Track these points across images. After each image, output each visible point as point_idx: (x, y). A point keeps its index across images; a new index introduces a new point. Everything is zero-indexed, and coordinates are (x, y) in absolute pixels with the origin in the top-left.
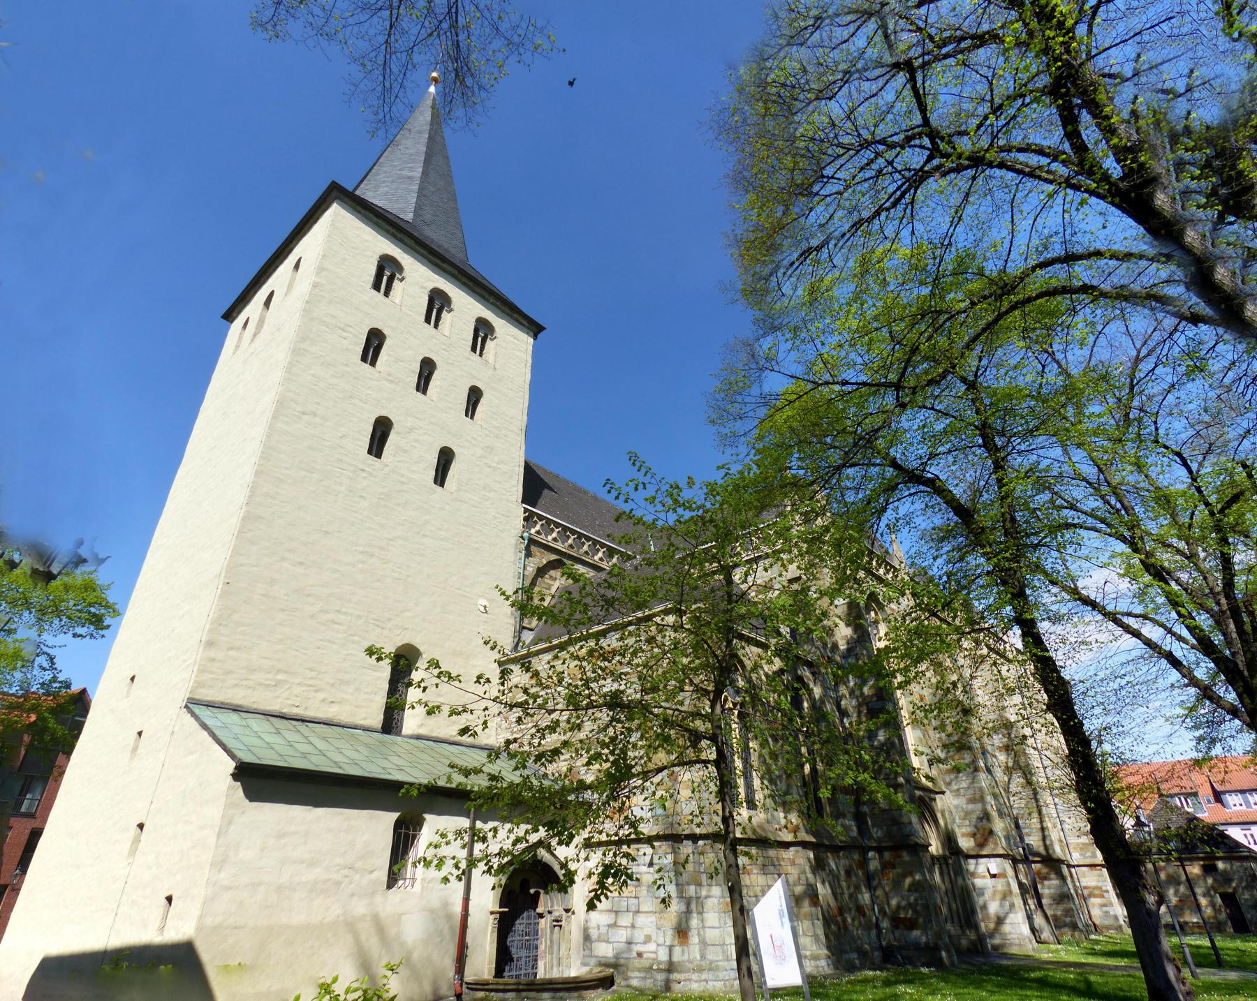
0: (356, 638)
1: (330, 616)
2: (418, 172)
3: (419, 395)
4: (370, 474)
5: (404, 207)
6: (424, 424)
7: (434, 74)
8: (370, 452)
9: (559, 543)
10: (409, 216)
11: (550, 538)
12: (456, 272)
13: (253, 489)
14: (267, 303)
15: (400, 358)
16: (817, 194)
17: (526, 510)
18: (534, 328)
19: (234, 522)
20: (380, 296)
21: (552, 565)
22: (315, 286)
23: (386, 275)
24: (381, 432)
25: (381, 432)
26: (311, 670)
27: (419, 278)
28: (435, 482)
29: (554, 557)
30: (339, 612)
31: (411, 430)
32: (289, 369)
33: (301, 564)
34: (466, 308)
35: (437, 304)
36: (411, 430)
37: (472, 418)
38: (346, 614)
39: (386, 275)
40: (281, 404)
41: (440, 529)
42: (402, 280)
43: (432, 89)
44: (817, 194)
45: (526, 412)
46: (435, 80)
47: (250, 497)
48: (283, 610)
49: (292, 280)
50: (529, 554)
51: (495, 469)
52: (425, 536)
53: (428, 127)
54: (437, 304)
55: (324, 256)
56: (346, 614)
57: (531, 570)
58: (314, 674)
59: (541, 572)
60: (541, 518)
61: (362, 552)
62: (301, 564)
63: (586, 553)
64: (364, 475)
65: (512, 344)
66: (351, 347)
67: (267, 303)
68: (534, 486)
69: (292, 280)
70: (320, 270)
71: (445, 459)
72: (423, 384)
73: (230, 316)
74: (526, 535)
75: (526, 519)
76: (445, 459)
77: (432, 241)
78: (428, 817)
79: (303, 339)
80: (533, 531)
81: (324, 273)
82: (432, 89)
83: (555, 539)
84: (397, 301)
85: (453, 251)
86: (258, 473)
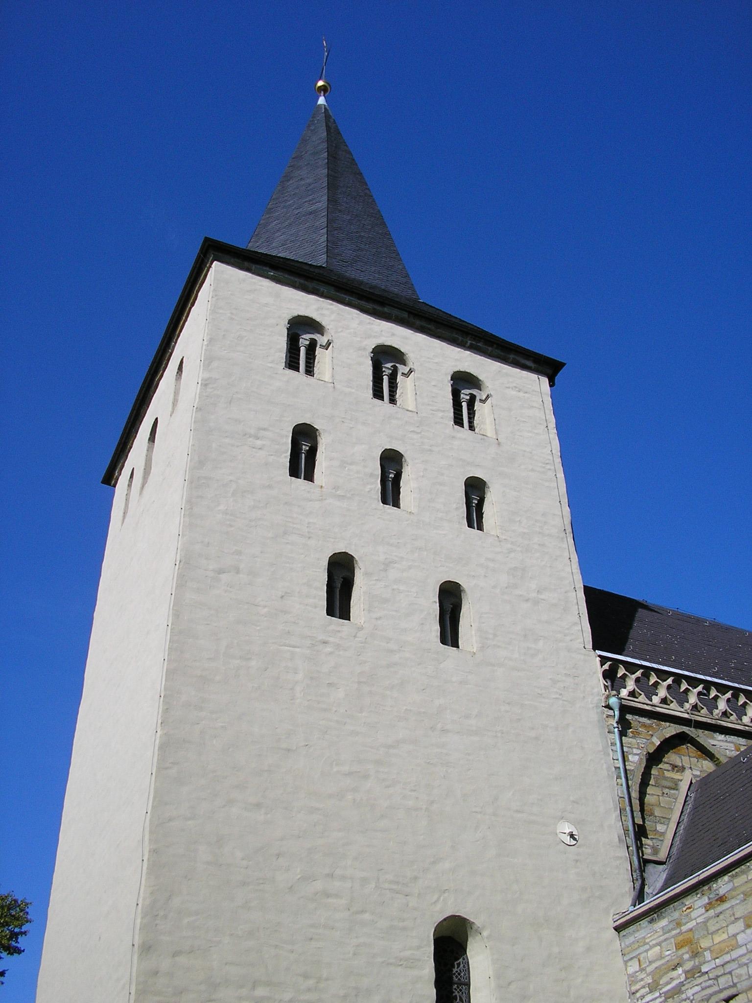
0: (367, 916)
1: (318, 885)
2: (322, 202)
3: (389, 509)
4: (338, 646)
5: (312, 250)
6: (407, 553)
7: (321, 83)
8: (330, 612)
9: (674, 705)
10: (321, 260)
11: (656, 700)
12: (405, 315)
13: (169, 698)
14: (152, 438)
15: (348, 461)
16: (648, 943)
17: (604, 660)
18: (548, 367)
19: (149, 756)
20: (299, 377)
21: (669, 744)
22: (205, 384)
23: (301, 345)
24: (341, 581)
25: (341, 581)
26: (306, 976)
27: (351, 332)
28: (443, 641)
29: (671, 730)
30: (331, 876)
31: (387, 565)
32: (191, 504)
33: (258, 806)
34: (432, 360)
35: (386, 364)
36: (387, 565)
37: (480, 528)
38: (343, 878)
39: (301, 345)
40: (187, 565)
41: (467, 717)
42: (327, 346)
43: (322, 101)
44: (648, 943)
45: (565, 501)
46: (324, 89)
47: (166, 711)
48: (244, 884)
49: (176, 393)
50: (624, 727)
51: (536, 602)
52: (444, 731)
53: (325, 145)
54: (386, 364)
55: (211, 340)
56: (343, 878)
57: (636, 760)
58: (311, 982)
59: (654, 758)
60: (631, 668)
61: (350, 774)
62: (258, 806)
63: (725, 714)
64: (329, 649)
65: (518, 400)
66: (271, 459)
67: (152, 438)
68: (611, 619)
69: (176, 393)
70: (208, 361)
71: (450, 598)
72: (391, 492)
73: (110, 478)
74: (613, 701)
75: (607, 675)
76: (450, 598)
77: (361, 283)
78: (235, 315)
79: (201, 463)
80: (624, 693)
81: (215, 364)
82: (322, 101)
83: (664, 701)
84: (327, 377)
85: (395, 290)
86: (170, 674)
